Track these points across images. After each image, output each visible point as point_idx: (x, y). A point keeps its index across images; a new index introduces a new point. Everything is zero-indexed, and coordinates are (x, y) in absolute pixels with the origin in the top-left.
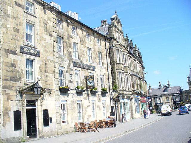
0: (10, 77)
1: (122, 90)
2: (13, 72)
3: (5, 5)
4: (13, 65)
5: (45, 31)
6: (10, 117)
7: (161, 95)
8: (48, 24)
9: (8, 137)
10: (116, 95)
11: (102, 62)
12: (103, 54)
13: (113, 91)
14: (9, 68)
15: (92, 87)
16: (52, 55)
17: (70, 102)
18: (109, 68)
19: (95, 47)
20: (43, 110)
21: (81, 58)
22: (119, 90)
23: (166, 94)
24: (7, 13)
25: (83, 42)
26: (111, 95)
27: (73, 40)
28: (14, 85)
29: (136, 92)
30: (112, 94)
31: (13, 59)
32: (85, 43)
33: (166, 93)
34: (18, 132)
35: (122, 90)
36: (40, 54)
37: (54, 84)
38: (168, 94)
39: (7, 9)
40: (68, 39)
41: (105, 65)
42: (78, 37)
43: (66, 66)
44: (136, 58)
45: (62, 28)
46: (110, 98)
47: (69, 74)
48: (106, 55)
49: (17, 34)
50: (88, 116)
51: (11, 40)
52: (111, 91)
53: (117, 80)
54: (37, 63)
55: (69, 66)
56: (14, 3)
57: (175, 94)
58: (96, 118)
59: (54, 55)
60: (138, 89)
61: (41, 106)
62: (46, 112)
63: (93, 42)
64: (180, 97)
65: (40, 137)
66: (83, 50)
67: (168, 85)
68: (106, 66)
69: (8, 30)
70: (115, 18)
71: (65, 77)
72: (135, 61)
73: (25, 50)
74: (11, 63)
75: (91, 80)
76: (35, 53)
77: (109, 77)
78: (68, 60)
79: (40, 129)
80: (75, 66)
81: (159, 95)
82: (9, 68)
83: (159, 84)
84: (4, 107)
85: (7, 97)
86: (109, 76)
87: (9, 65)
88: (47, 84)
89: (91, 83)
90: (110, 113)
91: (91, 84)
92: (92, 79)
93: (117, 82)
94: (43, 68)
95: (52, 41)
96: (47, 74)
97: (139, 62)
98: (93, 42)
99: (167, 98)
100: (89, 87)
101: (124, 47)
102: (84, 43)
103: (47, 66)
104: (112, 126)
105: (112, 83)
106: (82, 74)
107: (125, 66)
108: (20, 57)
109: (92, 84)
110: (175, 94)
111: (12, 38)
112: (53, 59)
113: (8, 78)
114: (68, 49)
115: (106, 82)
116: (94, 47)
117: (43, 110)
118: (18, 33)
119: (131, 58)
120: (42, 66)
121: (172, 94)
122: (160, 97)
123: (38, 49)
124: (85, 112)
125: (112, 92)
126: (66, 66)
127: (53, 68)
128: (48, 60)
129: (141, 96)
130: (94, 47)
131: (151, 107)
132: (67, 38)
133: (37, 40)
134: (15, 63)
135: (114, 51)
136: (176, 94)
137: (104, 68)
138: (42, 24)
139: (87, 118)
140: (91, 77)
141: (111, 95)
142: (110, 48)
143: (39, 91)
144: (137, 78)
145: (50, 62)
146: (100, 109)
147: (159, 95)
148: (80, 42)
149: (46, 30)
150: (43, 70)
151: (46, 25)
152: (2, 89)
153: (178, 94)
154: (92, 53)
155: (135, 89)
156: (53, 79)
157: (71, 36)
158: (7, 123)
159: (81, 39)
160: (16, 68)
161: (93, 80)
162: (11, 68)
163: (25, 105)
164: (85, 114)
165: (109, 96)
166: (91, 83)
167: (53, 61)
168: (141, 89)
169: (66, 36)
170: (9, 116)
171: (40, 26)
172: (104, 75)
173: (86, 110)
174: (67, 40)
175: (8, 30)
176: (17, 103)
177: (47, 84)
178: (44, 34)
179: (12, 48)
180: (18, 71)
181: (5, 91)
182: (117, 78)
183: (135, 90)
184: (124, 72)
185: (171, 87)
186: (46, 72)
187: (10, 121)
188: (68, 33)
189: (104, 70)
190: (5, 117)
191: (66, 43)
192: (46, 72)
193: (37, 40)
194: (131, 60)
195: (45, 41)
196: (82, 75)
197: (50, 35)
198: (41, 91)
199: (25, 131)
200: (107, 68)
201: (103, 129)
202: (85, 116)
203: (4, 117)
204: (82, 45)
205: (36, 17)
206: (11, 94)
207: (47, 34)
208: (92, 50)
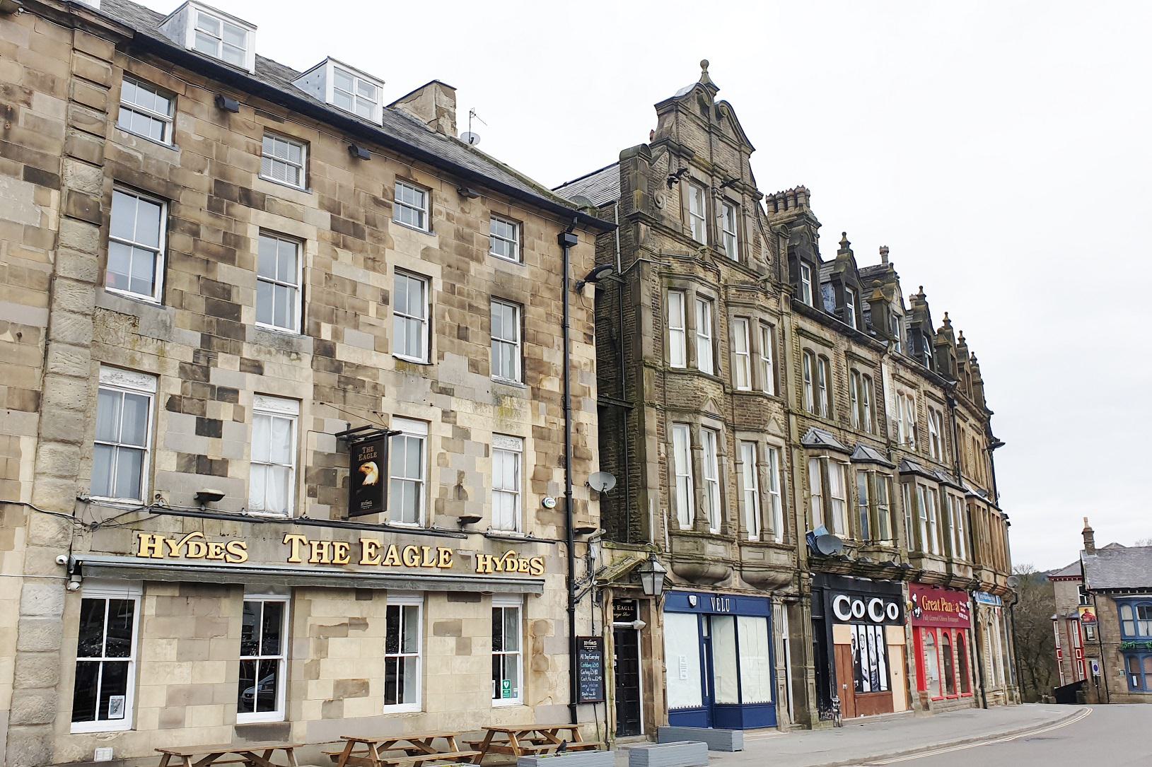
8: (22, 110)
16: (42, 298)
19: (463, 275)
37: (25, 473)
40: (214, 208)
47: (191, 421)
102: (368, 240)
127: (38, 372)
131: (805, 496)
139: (327, 703)
143: (659, 582)
148: (329, 234)
154: (431, 306)
167: (43, 332)
169: (198, 191)
174: (204, 218)
188: (222, 174)
194: (826, 360)
198: (664, 584)
200: (559, 399)
201: (1095, 540)
202: (312, 684)
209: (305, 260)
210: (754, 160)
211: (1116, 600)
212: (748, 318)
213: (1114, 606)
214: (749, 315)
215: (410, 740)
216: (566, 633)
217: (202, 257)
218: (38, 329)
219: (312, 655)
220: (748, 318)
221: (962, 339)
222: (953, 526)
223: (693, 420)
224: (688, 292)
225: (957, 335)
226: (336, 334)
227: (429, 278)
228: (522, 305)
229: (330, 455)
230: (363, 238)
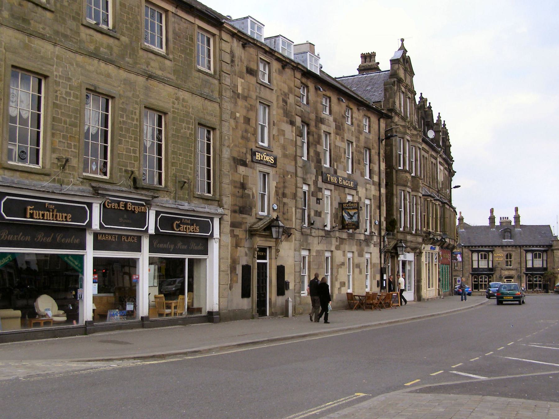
0: (239, 206)
1: (404, 233)
2: (242, 197)
3: (234, 76)
4: (243, 186)
5: (284, 116)
6: (237, 275)
7: (492, 246)
9: (235, 308)
10: (393, 243)
11: (370, 170)
12: (373, 152)
13: (388, 234)
14: (238, 192)
15: (353, 225)
16: (293, 163)
17: (314, 254)
18: (383, 182)
20: (278, 267)
21: (335, 164)
22: (397, 232)
23: (506, 246)
24: (237, 92)
25: (340, 130)
26: (382, 243)
27: (323, 128)
28: (244, 221)
29: (431, 237)
30: (384, 241)
31: (243, 173)
32: (344, 130)
33: (506, 241)
34: (246, 300)
35: (404, 233)
36: (278, 163)
38: (513, 246)
39: (236, 84)
40: (316, 126)
41: (375, 176)
42: (331, 119)
43: (311, 183)
44: (437, 152)
45: (308, 103)
46: (380, 248)
47: (315, 198)
48: (379, 153)
49: (248, 127)
50: (341, 283)
51: (240, 140)
52: (383, 233)
53: (395, 208)
54: (273, 180)
55: (316, 182)
56: (245, 70)
57: (533, 246)
58: (353, 289)
59: (296, 163)
60: (436, 230)
61: (276, 258)
62: (281, 270)
63: (357, 128)
64: (545, 258)
65: (272, 314)
66: (340, 147)
67: (517, 218)
68: (376, 179)
69: (237, 122)
70: (402, 60)
71: (309, 205)
72: (436, 159)
73: (258, 155)
74: (241, 182)
75: (352, 212)
76: (271, 162)
77: (382, 203)
78: (315, 170)
79: (273, 299)
80: (325, 182)
81: (485, 246)
82: (238, 192)
83: (489, 215)
84: (231, 258)
85: (235, 241)
86: (381, 201)
87: (239, 185)
88: (285, 219)
89: (351, 217)
90: (378, 281)
91: (351, 218)
92: (354, 209)
93: (395, 214)
94: (280, 188)
95: (294, 135)
96: (285, 200)
97: (444, 159)
98: (356, 125)
99: (509, 256)
100: (347, 225)
101: (415, 129)
103: (286, 184)
104: (503, 218)
105: (385, 216)
106: (335, 197)
107: (413, 174)
108: (251, 170)
109: (355, 219)
110: (533, 246)
111: (242, 136)
112: (294, 171)
113: (237, 208)
114: (316, 148)
115: (375, 213)
116: (358, 139)
117: (278, 267)
118: (249, 124)
119: (427, 152)
120: (279, 186)
121: (523, 246)
122: (488, 252)
123: (275, 153)
124: (337, 276)
125: (384, 237)
126: (311, 183)
127: (294, 187)
128: (288, 173)
129: (442, 247)
130: (358, 139)
132: (314, 125)
133: (274, 135)
134: (245, 182)
135: (394, 143)
136: (537, 246)
137: (374, 183)
138: (281, 103)
139: (339, 288)
140: (353, 205)
141: (382, 243)
142: (388, 138)
144: (437, 203)
145: (289, 176)
146: (361, 272)
147: (485, 246)
149: (286, 113)
150: (281, 192)
151: (286, 103)
152: (230, 227)
153: (540, 246)
155: (431, 230)
156: (294, 209)
157: (321, 118)
158: (234, 285)
159: (337, 123)
160: (246, 191)
161: (356, 211)
162: (241, 191)
163: (256, 256)
164: (337, 280)
165: (379, 245)
166: (351, 217)
168: (444, 231)
170: (237, 273)
171: (278, 107)
172: (372, 198)
173: (338, 272)
175: (237, 122)
176: (246, 252)
177: (285, 219)
178: (283, 122)
179: (242, 154)
180: (249, 195)
181: (233, 230)
182: (395, 204)
183: (429, 233)
184: (410, 190)
185: (523, 227)
186: (284, 195)
187: (237, 282)
189: (373, 187)
190: (233, 274)
191: (313, 135)
192: (284, 195)
193: (274, 135)
194: (426, 159)
195: (284, 135)
196: (335, 200)
197: (292, 123)
199: (254, 301)
200: (378, 184)
202: (336, 282)
203: (231, 273)
204: (338, 137)
205: (273, 90)
206: (240, 237)
207: (287, 122)
208: (354, 144)
209: (330, 140)
210: (415, 79)
211: (471, 251)
212: (415, 146)
213: (470, 253)
214: (415, 145)
215: (127, 343)
216: (471, 266)
217: (132, 56)
218: (293, 173)
219: (336, 274)
220: (415, 146)
221: (444, 125)
222: (431, 215)
223: (405, 189)
224: (404, 139)
225: (443, 123)
226: (337, 167)
227: (352, 143)
228: (369, 150)
229: (337, 208)
230: (341, 131)
